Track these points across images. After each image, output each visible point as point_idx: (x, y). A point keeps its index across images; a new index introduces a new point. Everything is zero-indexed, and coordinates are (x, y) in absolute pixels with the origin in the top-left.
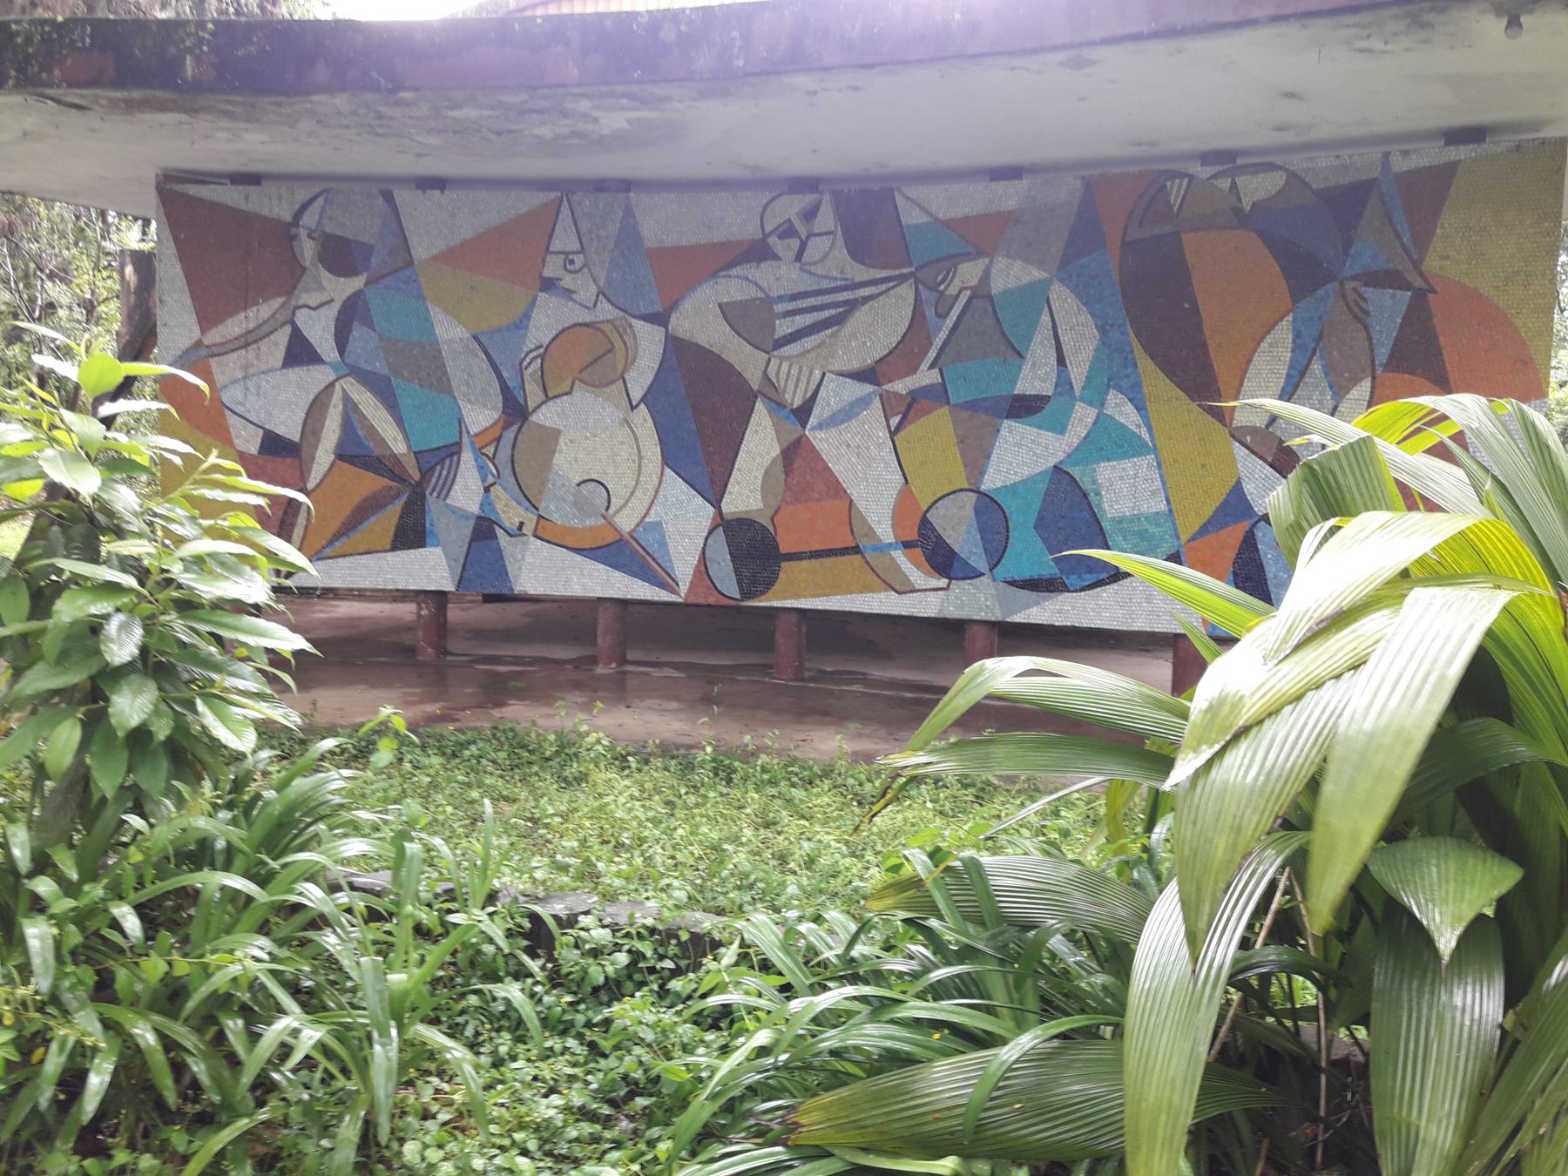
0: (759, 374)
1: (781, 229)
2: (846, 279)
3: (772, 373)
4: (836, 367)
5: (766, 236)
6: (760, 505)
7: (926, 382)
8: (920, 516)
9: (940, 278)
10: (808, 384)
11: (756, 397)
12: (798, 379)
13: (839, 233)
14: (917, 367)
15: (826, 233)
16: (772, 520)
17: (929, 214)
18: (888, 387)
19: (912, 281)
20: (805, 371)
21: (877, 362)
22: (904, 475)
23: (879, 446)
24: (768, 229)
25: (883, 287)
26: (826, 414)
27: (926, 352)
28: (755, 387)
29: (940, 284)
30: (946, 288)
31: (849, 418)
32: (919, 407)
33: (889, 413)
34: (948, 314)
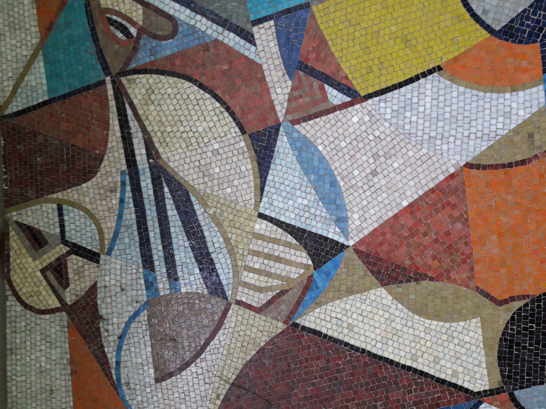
0: (259, 320)
1: (55, 283)
2: (123, 183)
3: (263, 298)
4: (250, 196)
5: (64, 307)
6: (475, 323)
7: (273, 47)
8: (498, 41)
9: (120, 35)
10: (275, 241)
11: (296, 325)
12: (269, 257)
13: (60, 195)
14: (252, 62)
15: (61, 215)
16: (500, 303)
17: (34, 56)
18: (281, 111)
19: (124, 80)
20: (258, 245)
21: (243, 131)
22: (424, 75)
23: (374, 120)
24: (54, 303)
25: (133, 124)
26: (321, 210)
27: (229, 50)
28: (281, 326)
29: (128, 34)
30: (133, 23)
31: (330, 173)
32: (313, 56)
33: (323, 107)
34: (170, 18)
